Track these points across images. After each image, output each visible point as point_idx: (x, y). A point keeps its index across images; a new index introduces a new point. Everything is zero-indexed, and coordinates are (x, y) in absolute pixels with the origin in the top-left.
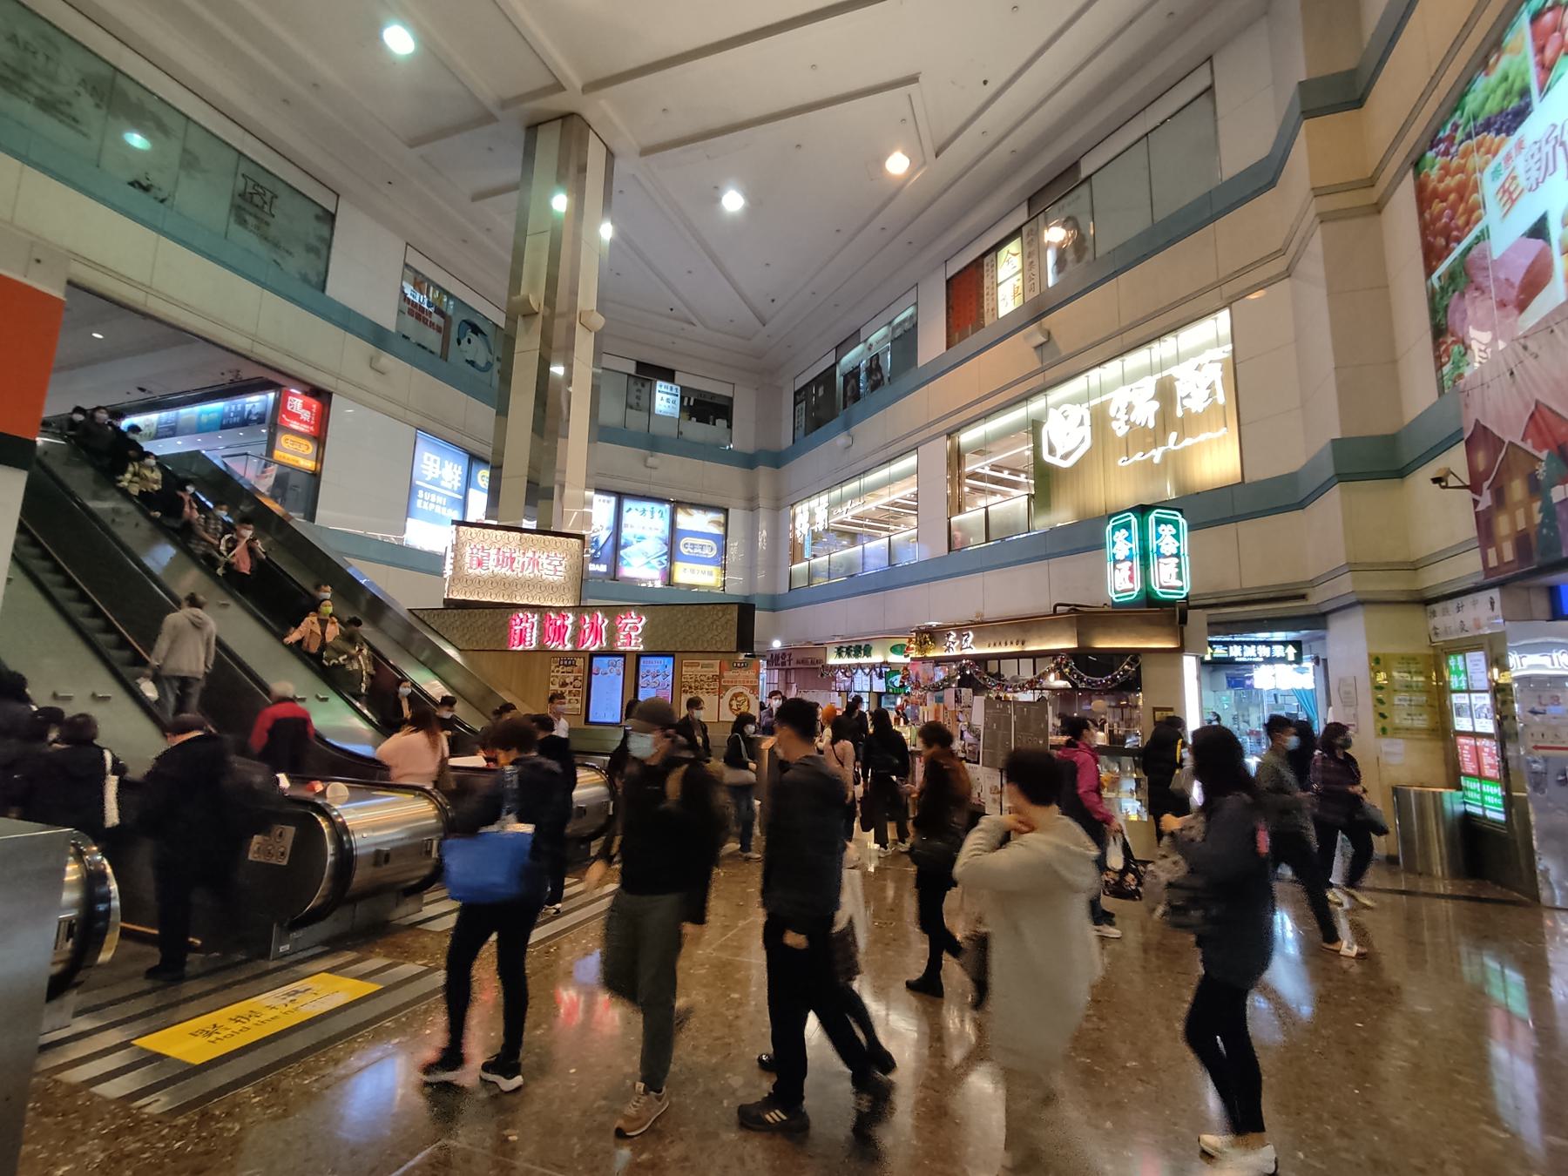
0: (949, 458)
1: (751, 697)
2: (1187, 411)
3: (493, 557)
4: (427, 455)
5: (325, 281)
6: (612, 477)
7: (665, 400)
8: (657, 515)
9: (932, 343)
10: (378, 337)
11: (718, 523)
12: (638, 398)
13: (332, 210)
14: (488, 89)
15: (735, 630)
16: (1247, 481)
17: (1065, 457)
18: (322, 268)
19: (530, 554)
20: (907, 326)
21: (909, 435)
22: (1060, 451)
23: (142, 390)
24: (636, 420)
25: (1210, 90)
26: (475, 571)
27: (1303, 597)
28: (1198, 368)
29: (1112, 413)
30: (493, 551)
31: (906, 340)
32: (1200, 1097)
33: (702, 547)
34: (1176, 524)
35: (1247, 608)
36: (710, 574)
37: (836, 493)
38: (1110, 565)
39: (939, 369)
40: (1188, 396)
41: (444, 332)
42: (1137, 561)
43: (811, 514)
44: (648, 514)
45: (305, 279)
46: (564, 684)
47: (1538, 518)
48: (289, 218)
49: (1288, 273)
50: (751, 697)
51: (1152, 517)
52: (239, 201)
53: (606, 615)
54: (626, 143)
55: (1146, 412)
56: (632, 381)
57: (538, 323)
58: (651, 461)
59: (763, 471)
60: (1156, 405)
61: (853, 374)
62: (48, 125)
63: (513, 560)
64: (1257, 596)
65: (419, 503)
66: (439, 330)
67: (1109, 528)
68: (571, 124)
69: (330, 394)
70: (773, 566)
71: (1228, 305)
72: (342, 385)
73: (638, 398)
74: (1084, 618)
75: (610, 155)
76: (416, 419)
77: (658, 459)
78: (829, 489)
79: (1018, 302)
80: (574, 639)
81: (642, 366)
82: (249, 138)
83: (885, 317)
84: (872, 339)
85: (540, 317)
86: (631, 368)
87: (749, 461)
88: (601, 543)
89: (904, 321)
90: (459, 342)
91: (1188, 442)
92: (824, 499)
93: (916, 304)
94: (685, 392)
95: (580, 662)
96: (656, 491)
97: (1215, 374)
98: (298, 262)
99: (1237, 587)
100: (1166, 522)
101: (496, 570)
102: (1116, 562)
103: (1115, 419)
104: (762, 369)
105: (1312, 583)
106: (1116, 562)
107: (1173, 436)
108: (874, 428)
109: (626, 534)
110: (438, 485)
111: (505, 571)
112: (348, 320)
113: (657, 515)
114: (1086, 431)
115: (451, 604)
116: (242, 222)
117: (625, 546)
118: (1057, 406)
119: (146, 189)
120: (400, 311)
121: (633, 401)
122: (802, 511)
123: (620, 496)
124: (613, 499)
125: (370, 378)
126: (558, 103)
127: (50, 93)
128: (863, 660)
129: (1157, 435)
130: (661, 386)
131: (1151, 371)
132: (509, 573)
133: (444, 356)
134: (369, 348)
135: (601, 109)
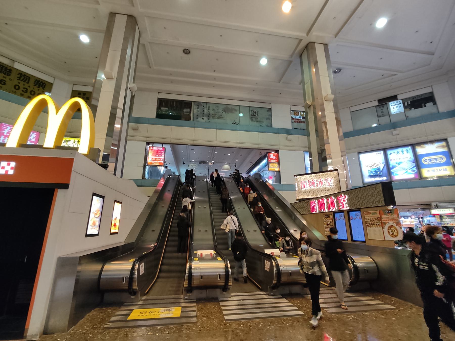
1: (398, 228)
3: (308, 184)
6: (379, 144)
8: (405, 152)
10: (287, 132)
11: (443, 147)
14: (285, 55)
15: (382, 195)
19: (319, 180)
24: (384, 120)
26: (304, 189)
30: (307, 182)
33: (436, 159)
44: (401, 153)
45: (268, 126)
46: (328, 225)
48: (262, 114)
50: (398, 228)
53: (335, 197)
54: (327, 37)
56: (378, 107)
58: (395, 132)
66: (304, 122)
72: (281, 147)
75: (326, 46)
81: (380, 101)
86: (376, 103)
88: (381, 169)
95: (331, 216)
98: (265, 123)
109: (392, 163)
112: (279, 131)
113: (405, 152)
115: (300, 200)
116: (252, 120)
117: (393, 168)
119: (235, 123)
121: (380, 114)
123: (385, 150)
124: (382, 152)
125: (288, 143)
126: (303, 44)
134: (285, 135)
135: (315, 36)
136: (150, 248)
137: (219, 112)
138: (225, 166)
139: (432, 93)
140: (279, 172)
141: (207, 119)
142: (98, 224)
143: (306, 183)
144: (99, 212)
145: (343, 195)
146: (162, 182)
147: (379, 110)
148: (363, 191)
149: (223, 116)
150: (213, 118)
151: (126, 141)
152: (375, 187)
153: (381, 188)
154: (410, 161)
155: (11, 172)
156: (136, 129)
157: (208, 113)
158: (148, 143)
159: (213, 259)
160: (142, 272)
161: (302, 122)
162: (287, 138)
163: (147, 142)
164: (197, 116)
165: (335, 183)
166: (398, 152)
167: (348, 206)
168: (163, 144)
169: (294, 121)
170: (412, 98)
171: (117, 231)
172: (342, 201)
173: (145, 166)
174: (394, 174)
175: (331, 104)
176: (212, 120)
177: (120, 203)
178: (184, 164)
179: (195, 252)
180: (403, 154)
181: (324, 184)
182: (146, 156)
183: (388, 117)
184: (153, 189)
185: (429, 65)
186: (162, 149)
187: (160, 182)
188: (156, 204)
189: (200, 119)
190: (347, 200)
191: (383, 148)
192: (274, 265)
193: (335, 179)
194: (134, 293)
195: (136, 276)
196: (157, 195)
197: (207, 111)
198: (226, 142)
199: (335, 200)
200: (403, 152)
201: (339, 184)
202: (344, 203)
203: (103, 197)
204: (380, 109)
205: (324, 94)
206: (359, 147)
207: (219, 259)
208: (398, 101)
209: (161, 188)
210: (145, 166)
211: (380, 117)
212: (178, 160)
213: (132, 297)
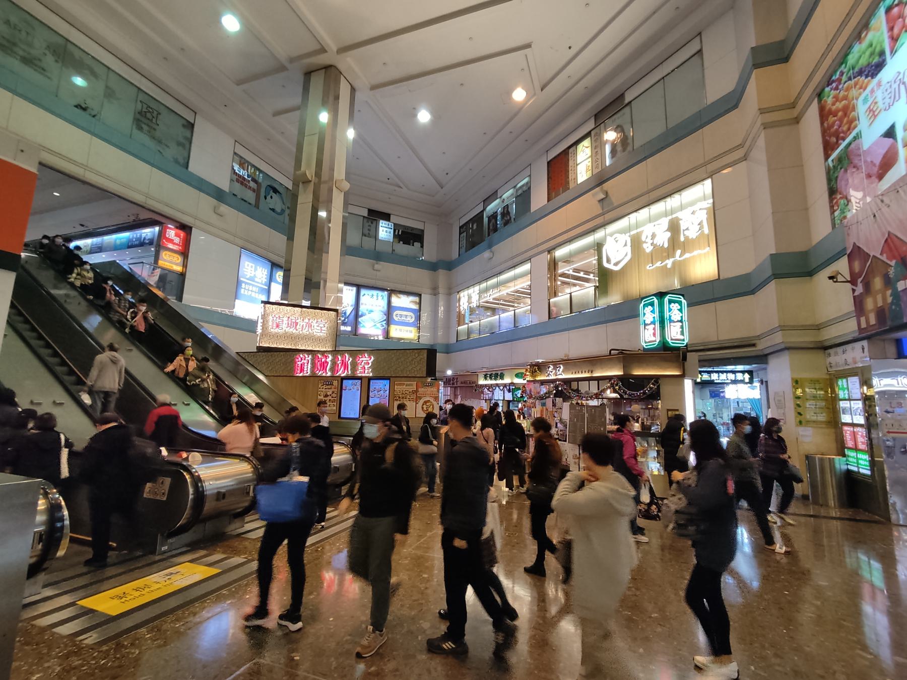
0: (549, 265)
1: (435, 403)
2: (686, 238)
3: (285, 322)
4: (247, 263)
5: (188, 163)
6: (354, 276)
7: (385, 231)
8: (380, 298)
9: (539, 198)
10: (219, 195)
11: (415, 302)
12: (369, 230)
13: (192, 121)
14: (282, 51)
15: (425, 364)
16: (721, 278)
17: (616, 264)
18: (186, 155)
19: (306, 320)
20: (525, 188)
21: (526, 252)
22: (613, 261)
23: (82, 225)
24: (368, 243)
25: (700, 52)
26: (275, 330)
27: (754, 345)
28: (693, 213)
29: (643, 239)
30: (285, 319)
31: (524, 197)
32: (694, 635)
33: (406, 316)
34: (680, 303)
35: (721, 352)
36: (411, 332)
37: (484, 285)
38: (642, 327)
39: (543, 214)
40: (687, 229)
41: (257, 192)
42: (658, 324)
43: (469, 297)
44: (375, 297)
45: (176, 161)
46: (326, 396)
47: (890, 300)
48: (167, 126)
49: (745, 158)
50: (435, 403)
51: (667, 299)
52: (138, 116)
53: (350, 356)
54: (362, 83)
55: (663, 239)
56: (366, 220)
57: (311, 187)
58: (376, 266)
59: (442, 273)
60: (668, 234)
61: (494, 216)
62: (28, 72)
63: (297, 324)
64: (727, 345)
65: (242, 291)
66: (254, 191)
67: (642, 305)
68: (330, 71)
69: (191, 228)
70: (447, 327)
71: (711, 176)
72: (198, 223)
73: (369, 230)
74: (627, 357)
75: (353, 90)
76: (241, 242)
77: (381, 265)
78: (480, 283)
79: (589, 174)
80: (332, 370)
81: (371, 212)
82: (144, 80)
83: (512, 183)
84: (505, 196)
85: (312, 183)
86: (365, 213)
87: (433, 267)
88: (348, 314)
89: (523, 186)
90: (266, 198)
91: (687, 255)
92: (477, 288)
93: (530, 176)
94: (396, 227)
95: (335, 383)
96: (380, 284)
97: (703, 216)
98: (172, 151)
99: (716, 339)
100: (675, 302)
101: (287, 330)
102: (646, 325)
103: (645, 242)
104: (441, 213)
105: (759, 337)
106: (646, 325)
107: (678, 252)
108: (505, 247)
109: (362, 309)
110: (253, 281)
111: (292, 330)
112: (201, 185)
113: (380, 298)
114: (628, 249)
115: (261, 349)
116: (140, 129)
117: (362, 316)
118: (611, 235)
119: (85, 109)
120: (232, 180)
121: (366, 232)
122: (464, 296)
123: (359, 287)
124: (355, 289)
125: (214, 218)
126: (323, 59)
127: (29, 53)
128: (499, 382)
129: (669, 251)
130: (382, 223)
131: (666, 214)
132: (294, 331)
133: (257, 206)
134: (214, 201)
135: (347, 63)
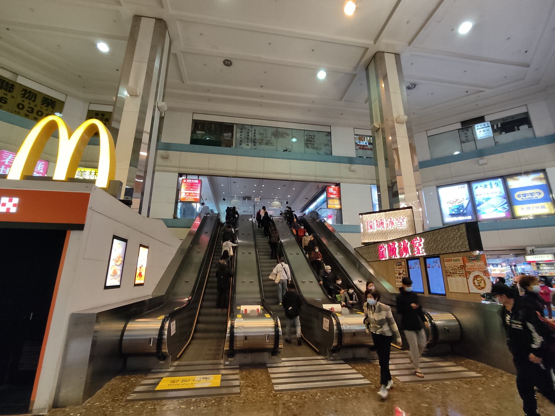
1: (485, 278)
3: (375, 224)
6: (462, 176)
8: (494, 186)
10: (350, 161)
11: (540, 179)
14: (348, 68)
15: (466, 238)
19: (390, 220)
24: (469, 147)
26: (370, 231)
30: (375, 222)
33: (532, 194)
44: (489, 187)
45: (327, 154)
46: (400, 274)
48: (320, 139)
50: (485, 278)
53: (409, 241)
54: (399, 45)
56: (461, 131)
58: (481, 161)
66: (371, 149)
72: (343, 180)
75: (397, 56)
81: (463, 123)
86: (459, 126)
88: (465, 206)
95: (403, 263)
98: (324, 150)
109: (478, 199)
112: (340, 160)
113: (494, 186)
115: (366, 244)
116: (308, 147)
117: (479, 205)
119: (286, 151)
121: (463, 139)
123: (469, 183)
124: (466, 185)
125: (351, 175)
126: (369, 54)
134: (348, 165)
135: (384, 43)
136: (183, 303)
137: (267, 137)
138: (274, 202)
139: (527, 113)
140: (341, 209)
141: (252, 145)
142: (119, 273)
143: (374, 224)
144: (121, 259)
145: (418, 238)
146: (198, 222)
147: (463, 134)
148: (443, 234)
149: (272, 142)
150: (260, 143)
151: (154, 173)
152: (458, 229)
153: (464, 229)
154: (500, 196)
155: (13, 210)
156: (166, 158)
157: (253, 137)
158: (181, 175)
159: (260, 316)
160: (173, 332)
161: (368, 149)
162: (350, 168)
163: (179, 174)
164: (241, 141)
165: (409, 224)
166: (486, 186)
167: (425, 252)
168: (199, 175)
169: (358, 147)
170: (503, 119)
171: (142, 282)
172: (417, 245)
173: (176, 203)
174: (481, 212)
175: (404, 127)
176: (258, 146)
177: (147, 247)
178: (224, 200)
179: (238, 308)
180: (492, 187)
181: (395, 224)
182: (178, 191)
183: (473, 143)
184: (186, 231)
185: (524, 79)
186: (197, 181)
187: (195, 222)
188: (190, 249)
189: (244, 146)
190: (423, 244)
191: (468, 180)
192: (335, 323)
193: (408, 219)
194: (164, 357)
195: (165, 337)
196: (192, 238)
197: (253, 136)
198: (275, 173)
199: (409, 243)
200: (491, 185)
201: (413, 225)
202: (420, 248)
203: (125, 240)
204: (463, 133)
205: (395, 115)
206: (437, 180)
207: (268, 315)
208: (486, 123)
209: (196, 230)
210: (176, 203)
211: (464, 142)
212: (217, 196)
213: (161, 362)
